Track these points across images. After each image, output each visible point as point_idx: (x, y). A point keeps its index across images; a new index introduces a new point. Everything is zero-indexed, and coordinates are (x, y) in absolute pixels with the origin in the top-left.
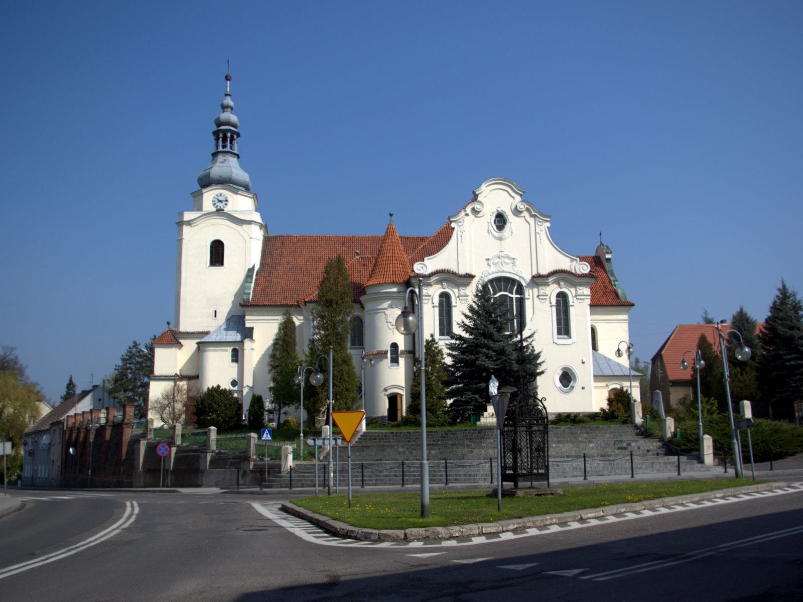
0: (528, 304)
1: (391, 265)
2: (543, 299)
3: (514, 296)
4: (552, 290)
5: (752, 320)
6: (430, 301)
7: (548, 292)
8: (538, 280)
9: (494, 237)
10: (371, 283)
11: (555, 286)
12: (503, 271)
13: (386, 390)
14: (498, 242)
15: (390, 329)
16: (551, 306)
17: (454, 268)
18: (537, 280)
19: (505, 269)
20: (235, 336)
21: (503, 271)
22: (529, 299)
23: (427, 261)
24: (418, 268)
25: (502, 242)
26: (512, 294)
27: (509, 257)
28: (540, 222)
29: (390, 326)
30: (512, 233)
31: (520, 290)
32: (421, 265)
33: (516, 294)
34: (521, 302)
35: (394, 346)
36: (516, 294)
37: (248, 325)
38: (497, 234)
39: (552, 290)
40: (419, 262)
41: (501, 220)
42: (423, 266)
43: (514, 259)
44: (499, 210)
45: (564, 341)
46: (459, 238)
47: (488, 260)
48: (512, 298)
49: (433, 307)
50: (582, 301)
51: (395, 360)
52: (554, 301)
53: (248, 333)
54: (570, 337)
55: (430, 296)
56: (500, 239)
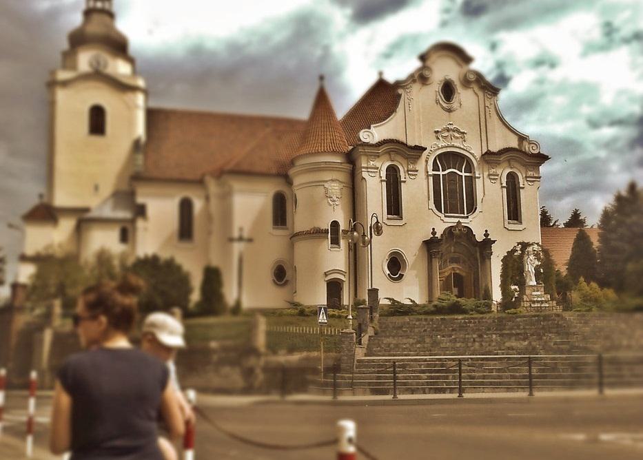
0: (479, 184)
1: (328, 133)
2: (412, 175)
3: (463, 174)
4: (503, 172)
5: (612, 206)
6: (378, 176)
7: (499, 172)
8: (489, 158)
9: (443, 108)
10: (303, 151)
11: (506, 164)
12: (453, 146)
13: (326, 274)
14: (447, 113)
15: (330, 205)
16: (502, 187)
17: (402, 138)
18: (487, 158)
19: (456, 144)
20: (124, 214)
21: (453, 146)
22: (479, 178)
23: (373, 129)
24: (364, 136)
25: (451, 113)
26: (461, 172)
27: (458, 131)
28: (489, 95)
29: (331, 202)
30: (461, 104)
31: (470, 168)
32: (368, 133)
33: (465, 172)
34: (471, 181)
35: (335, 225)
36: (465, 172)
37: (140, 200)
38: (444, 105)
39: (503, 172)
40: (364, 130)
41: (448, 90)
42: (370, 134)
43: (463, 133)
44: (447, 78)
45: (96, 140)
46: (407, 108)
47: (437, 132)
48: (462, 176)
49: (382, 181)
50: (414, 177)
51: (335, 241)
52: (383, 174)
53: (141, 211)
54: (521, 223)
55: (378, 168)
56: (449, 111)
